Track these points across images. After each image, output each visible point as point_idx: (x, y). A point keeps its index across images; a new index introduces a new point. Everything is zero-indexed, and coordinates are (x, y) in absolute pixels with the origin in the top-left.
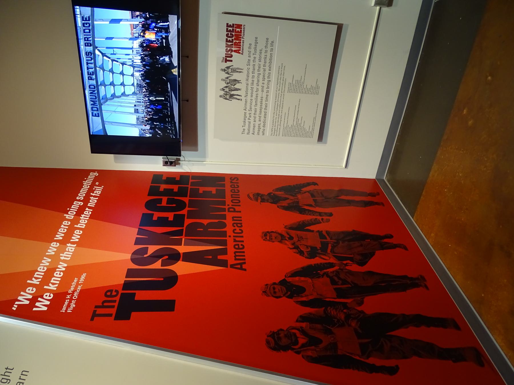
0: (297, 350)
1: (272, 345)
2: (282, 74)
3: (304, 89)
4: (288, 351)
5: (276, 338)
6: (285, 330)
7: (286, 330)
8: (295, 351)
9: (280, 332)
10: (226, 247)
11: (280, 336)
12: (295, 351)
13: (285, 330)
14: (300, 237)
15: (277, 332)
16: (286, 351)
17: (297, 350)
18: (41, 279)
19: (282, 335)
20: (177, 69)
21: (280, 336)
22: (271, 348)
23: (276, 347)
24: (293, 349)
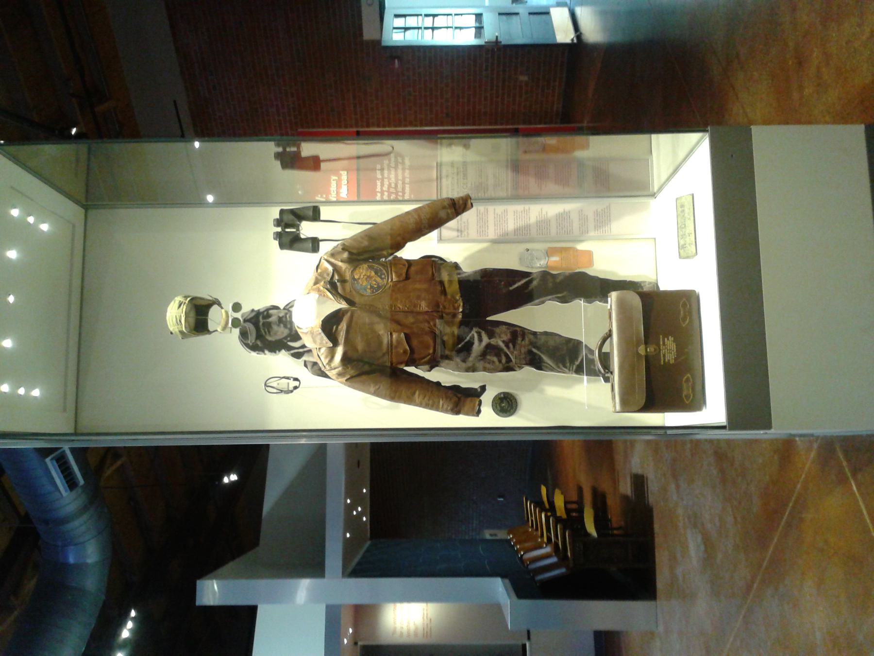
0: (296, 351)
1: (252, 339)
2: (549, 233)
3: (498, 216)
4: (279, 351)
5: (261, 324)
6: (282, 308)
7: (284, 309)
8: (292, 352)
9: (271, 312)
10: (265, 321)
11: (270, 320)
12: (292, 352)
13: (282, 308)
14: (383, 276)
15: (265, 313)
16: (275, 352)
17: (296, 351)
18: (579, 11)
19: (273, 319)
20: (406, 182)
21: (270, 320)
22: (247, 345)
23: (259, 343)
24: (289, 348)
